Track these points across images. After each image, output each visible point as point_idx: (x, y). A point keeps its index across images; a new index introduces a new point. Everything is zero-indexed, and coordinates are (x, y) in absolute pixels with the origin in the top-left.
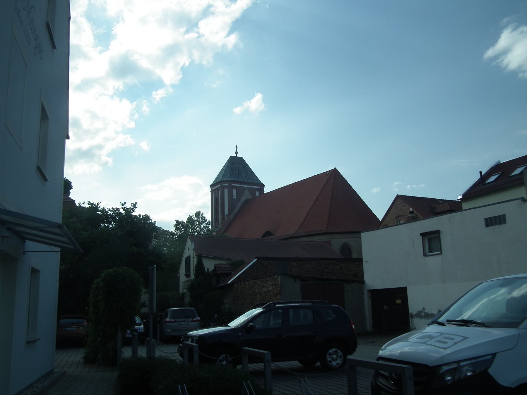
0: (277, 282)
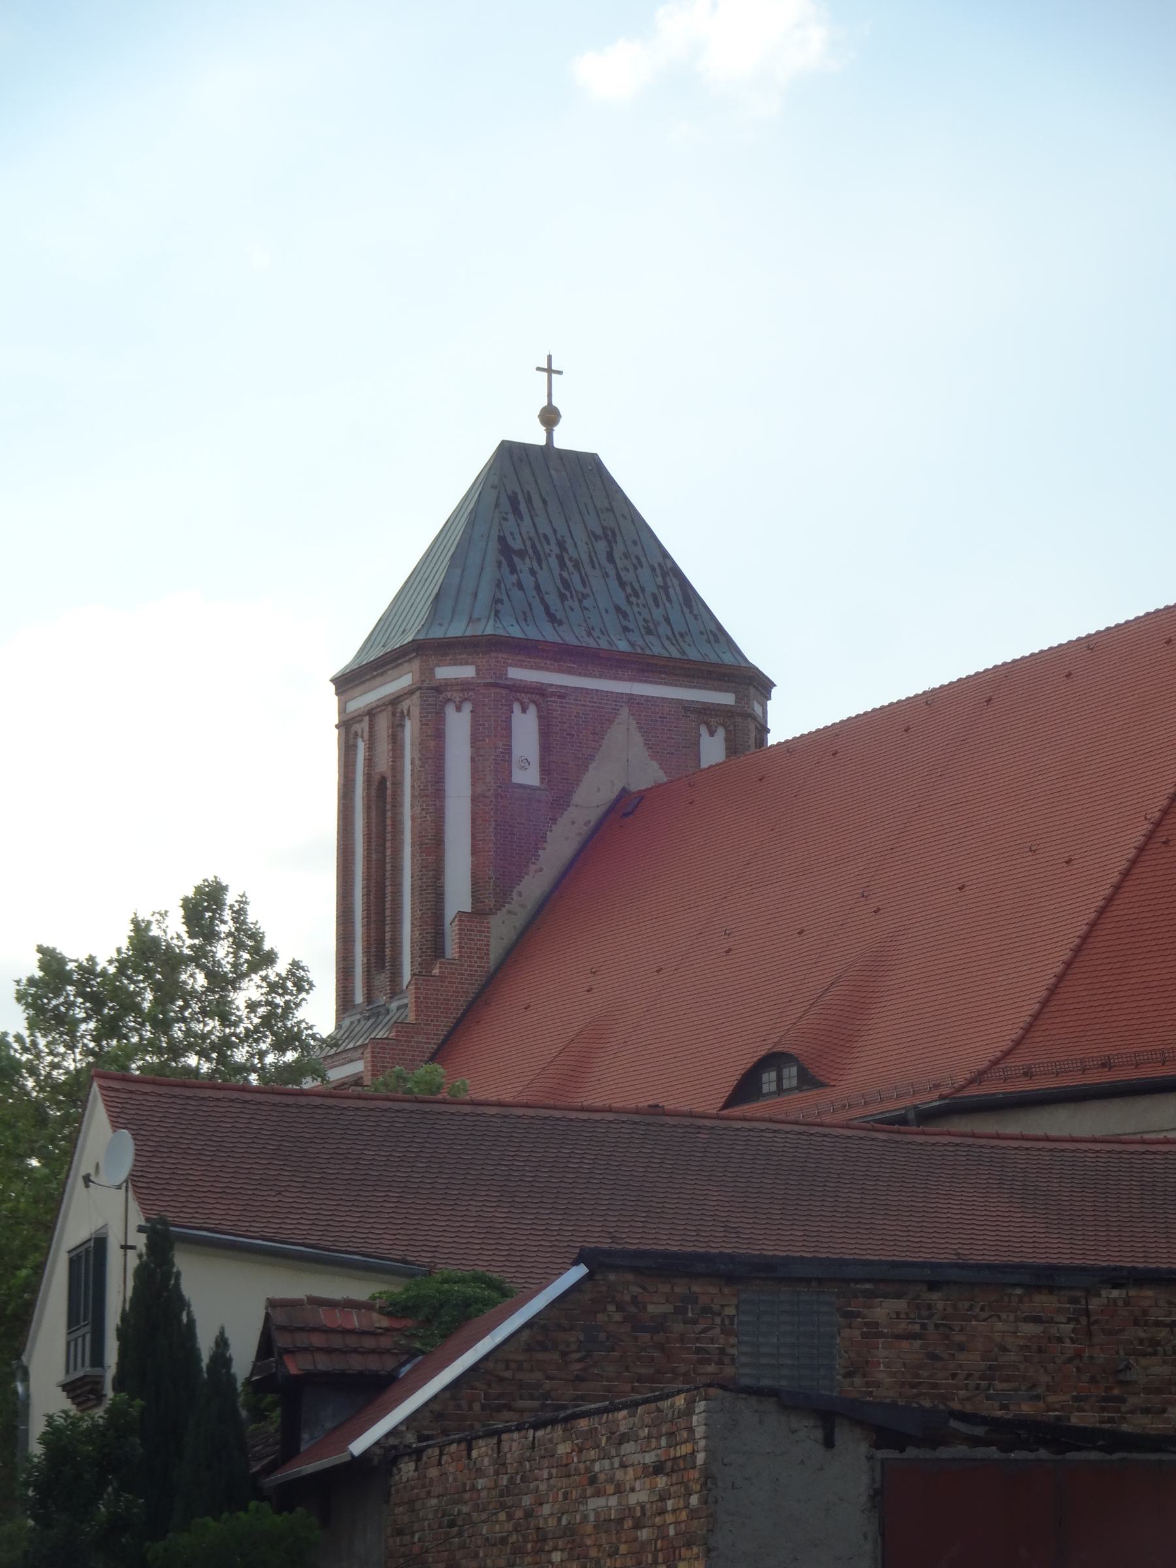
0: (684, 1449)
